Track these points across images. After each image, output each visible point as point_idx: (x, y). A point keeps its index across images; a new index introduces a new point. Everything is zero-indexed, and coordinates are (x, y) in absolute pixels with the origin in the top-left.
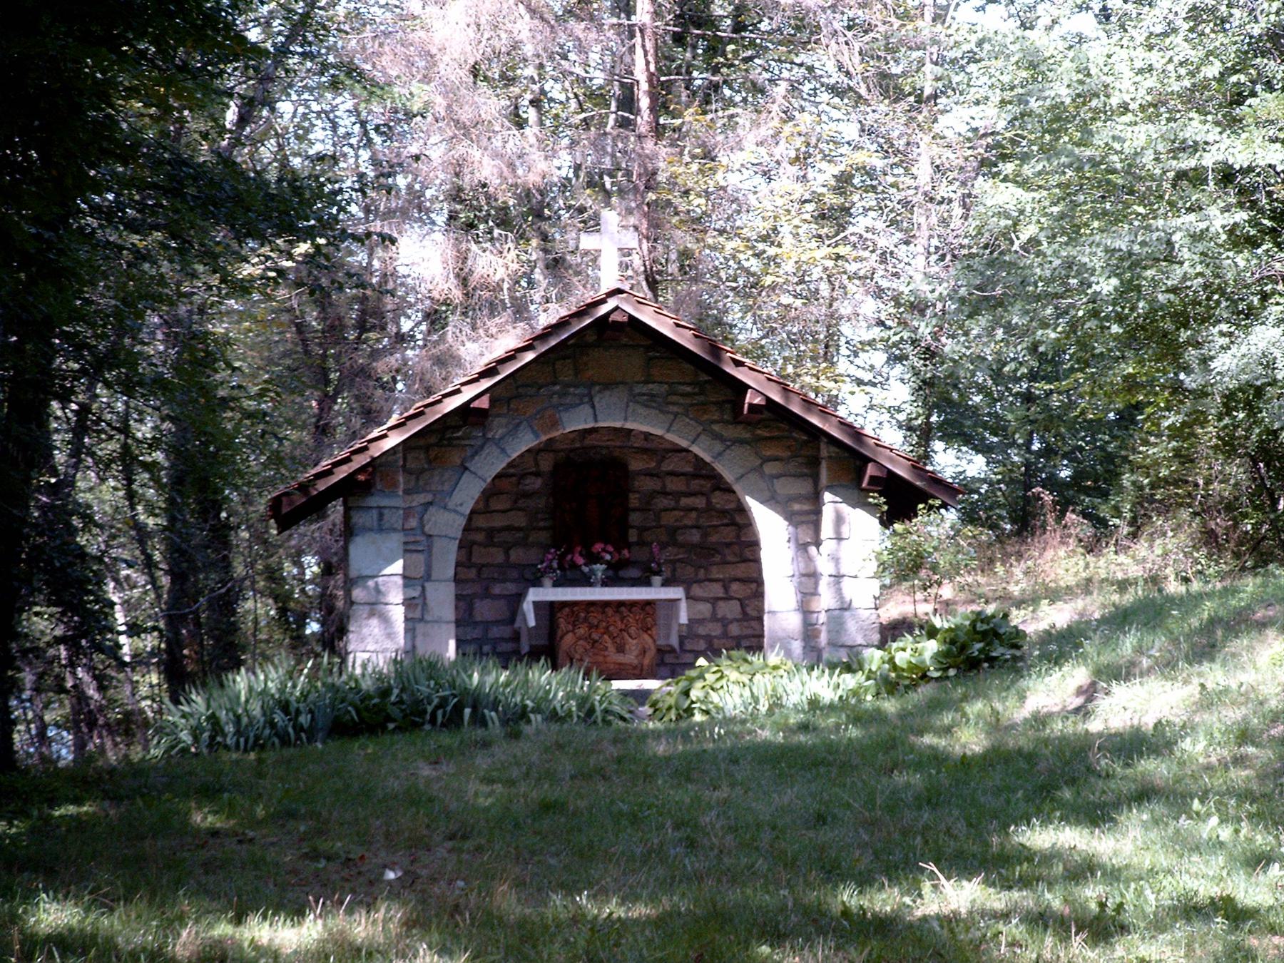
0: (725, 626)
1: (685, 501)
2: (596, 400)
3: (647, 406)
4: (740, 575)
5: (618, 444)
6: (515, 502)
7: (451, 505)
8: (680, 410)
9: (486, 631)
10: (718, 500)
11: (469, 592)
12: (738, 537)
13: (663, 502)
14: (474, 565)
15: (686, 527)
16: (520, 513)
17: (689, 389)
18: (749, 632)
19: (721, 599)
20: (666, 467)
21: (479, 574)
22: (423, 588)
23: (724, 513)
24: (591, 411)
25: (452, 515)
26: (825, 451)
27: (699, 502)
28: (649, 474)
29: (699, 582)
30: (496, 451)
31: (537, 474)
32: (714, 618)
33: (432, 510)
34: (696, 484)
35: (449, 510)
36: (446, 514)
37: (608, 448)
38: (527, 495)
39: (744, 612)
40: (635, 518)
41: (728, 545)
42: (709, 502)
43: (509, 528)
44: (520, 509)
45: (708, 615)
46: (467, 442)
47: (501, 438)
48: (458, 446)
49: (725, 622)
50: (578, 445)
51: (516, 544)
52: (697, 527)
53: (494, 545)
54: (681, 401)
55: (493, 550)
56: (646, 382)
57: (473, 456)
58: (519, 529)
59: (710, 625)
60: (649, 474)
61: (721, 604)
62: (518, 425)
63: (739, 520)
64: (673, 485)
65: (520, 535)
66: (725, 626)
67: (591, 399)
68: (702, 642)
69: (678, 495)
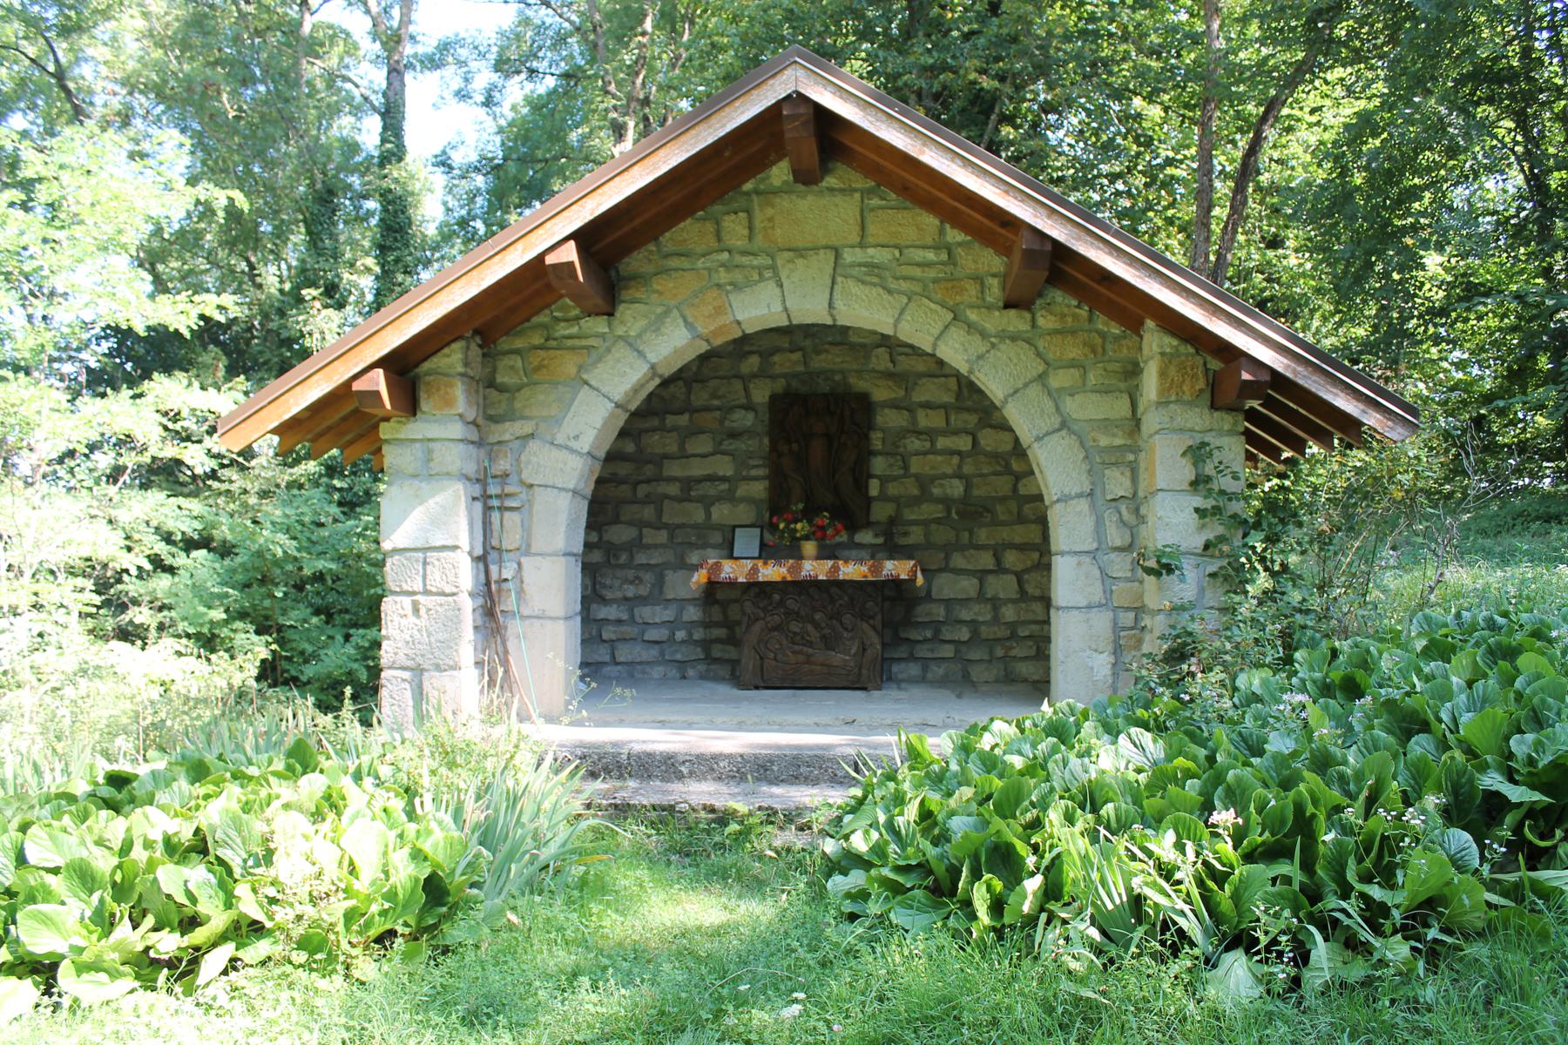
0: (996, 609)
1: (942, 443)
2: (783, 275)
3: (864, 283)
4: (1018, 540)
5: (855, 367)
6: (720, 444)
7: (560, 439)
8: (917, 288)
9: (681, 611)
10: (988, 439)
11: (660, 560)
12: (1015, 489)
13: (914, 444)
14: (666, 526)
15: (945, 476)
16: (726, 458)
17: (931, 256)
18: (1030, 617)
19: (990, 572)
20: (919, 396)
21: (671, 537)
22: (519, 564)
23: (995, 456)
24: (778, 290)
25: (564, 454)
26: (1155, 341)
27: (964, 443)
28: (895, 405)
29: (962, 548)
30: (631, 356)
31: (749, 407)
32: (981, 597)
33: (533, 445)
34: (957, 420)
35: (559, 446)
36: (555, 453)
37: (842, 372)
38: (734, 435)
39: (1022, 590)
40: (879, 465)
41: (1003, 499)
42: (975, 443)
43: (711, 478)
44: (723, 453)
45: (973, 593)
46: (584, 343)
47: (639, 336)
48: (573, 348)
49: (996, 603)
50: (801, 368)
51: (719, 499)
52: (960, 477)
53: (690, 500)
54: (917, 272)
55: (690, 506)
56: (862, 245)
57: (594, 364)
58: (723, 479)
59: (976, 608)
60: (895, 405)
61: (991, 579)
62: (667, 313)
63: (1016, 466)
64: (925, 420)
65: (725, 486)
66: (996, 609)
67: (776, 275)
68: (965, 629)
69: (931, 434)
